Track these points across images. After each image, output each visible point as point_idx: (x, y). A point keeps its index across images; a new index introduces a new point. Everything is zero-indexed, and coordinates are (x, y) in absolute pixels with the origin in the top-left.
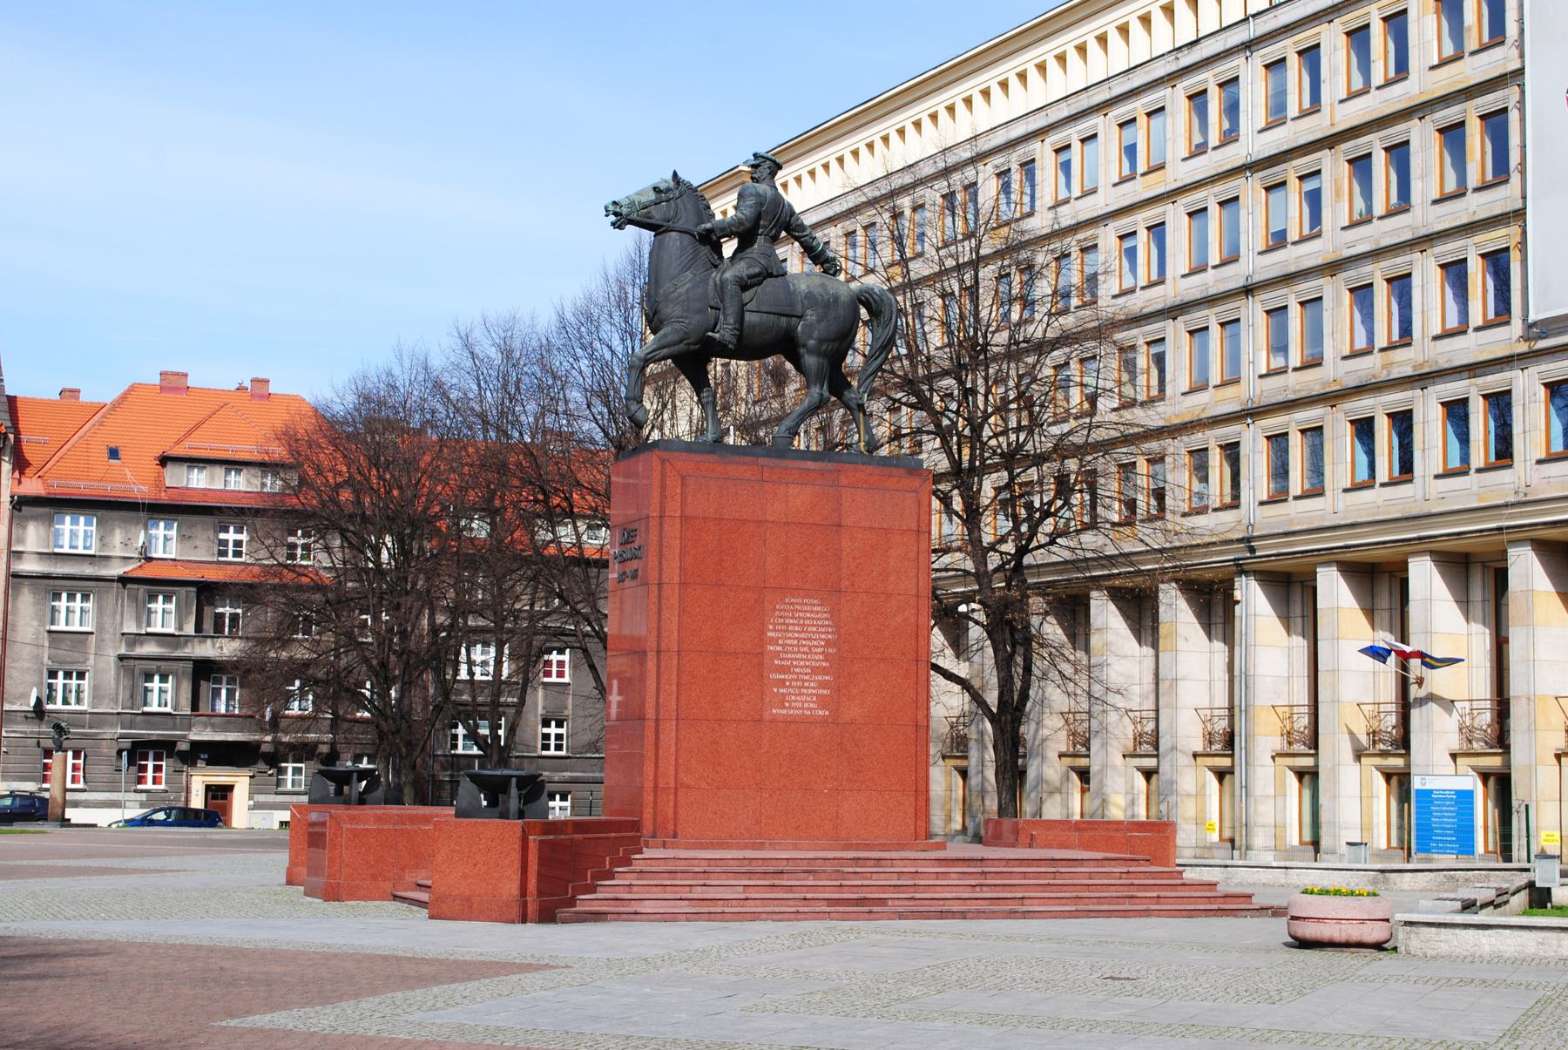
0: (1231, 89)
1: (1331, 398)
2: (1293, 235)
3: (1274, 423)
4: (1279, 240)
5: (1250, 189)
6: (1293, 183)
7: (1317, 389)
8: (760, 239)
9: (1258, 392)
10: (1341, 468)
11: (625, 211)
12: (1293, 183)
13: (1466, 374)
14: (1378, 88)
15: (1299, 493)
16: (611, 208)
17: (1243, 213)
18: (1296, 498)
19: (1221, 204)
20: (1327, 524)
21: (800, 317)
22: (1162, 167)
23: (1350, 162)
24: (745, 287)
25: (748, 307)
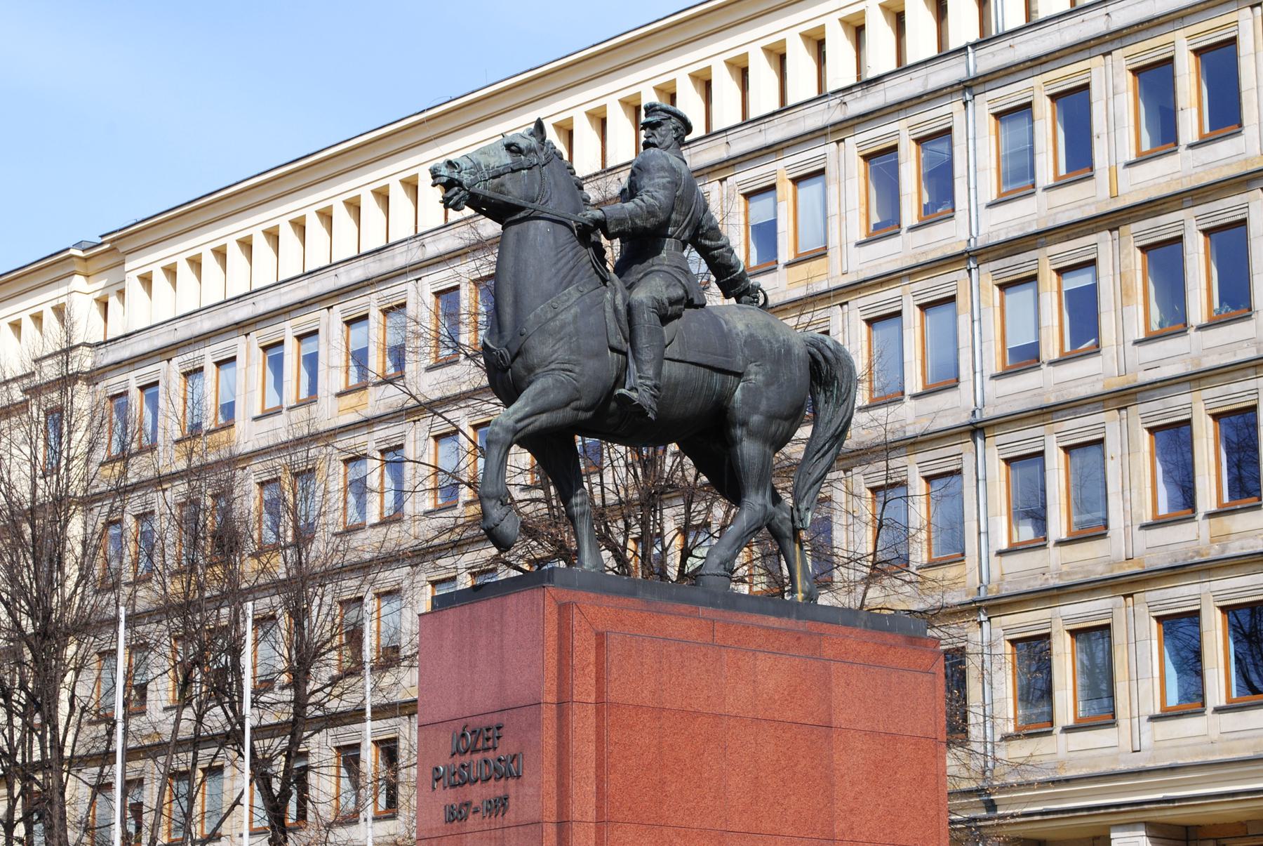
0: (940, 146)
1: (1126, 584)
2: (1050, 350)
3: (1027, 621)
4: (1025, 358)
5: (978, 289)
6: (1048, 279)
7: (1100, 572)
8: (669, 244)
9: (995, 574)
10: (1145, 686)
11: (466, 178)
12: (1048, 279)
14: (1191, 146)
15: (1070, 722)
16: (445, 172)
17: (964, 321)
18: (1067, 730)
19: (924, 307)
20: (1122, 767)
21: (739, 375)
22: (822, 254)
23: (1144, 249)
24: (665, 319)
25: (668, 352)
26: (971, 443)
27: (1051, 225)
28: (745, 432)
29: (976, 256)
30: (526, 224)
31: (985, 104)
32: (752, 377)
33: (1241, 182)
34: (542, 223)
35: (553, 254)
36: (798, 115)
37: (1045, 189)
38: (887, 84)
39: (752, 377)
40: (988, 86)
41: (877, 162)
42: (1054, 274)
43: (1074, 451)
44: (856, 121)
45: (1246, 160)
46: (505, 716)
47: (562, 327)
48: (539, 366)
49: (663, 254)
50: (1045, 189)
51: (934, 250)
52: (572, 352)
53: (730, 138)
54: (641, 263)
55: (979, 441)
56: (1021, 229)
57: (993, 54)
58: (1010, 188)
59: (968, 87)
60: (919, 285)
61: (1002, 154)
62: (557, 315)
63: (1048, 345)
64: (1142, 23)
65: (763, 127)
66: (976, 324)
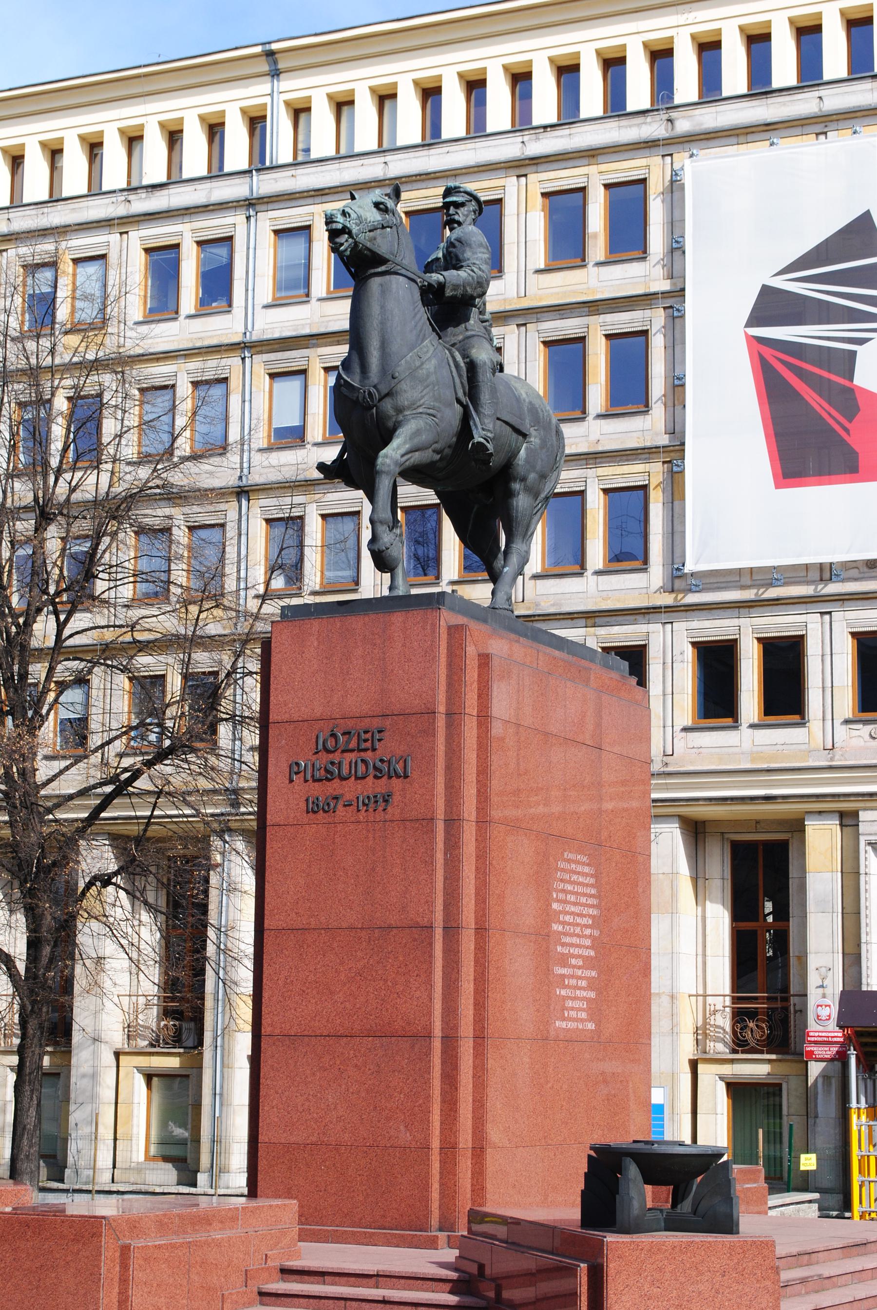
13: (582, 622)
26: (236, 503)
27: (323, 330)
28: (522, 487)
29: (251, 347)
30: (388, 277)
31: (267, 221)
32: (532, 439)
33: (500, 317)
34: (401, 278)
35: (412, 308)
36: (81, 205)
37: (319, 300)
38: (172, 191)
39: (532, 439)
40: (270, 206)
41: (156, 256)
42: (322, 371)
43: (330, 519)
44: (143, 218)
45: (505, 300)
46: (388, 722)
47: (428, 376)
48: (409, 408)
49: (472, 322)
50: (319, 300)
51: (210, 337)
52: (436, 400)
53: (11, 216)
54: (457, 325)
55: (244, 502)
56: (294, 330)
57: (276, 180)
58: (283, 294)
59: (252, 204)
60: (194, 365)
61: (279, 265)
62: (422, 364)
63: (313, 429)
64: (420, 175)
65: (45, 210)
66: (247, 404)
